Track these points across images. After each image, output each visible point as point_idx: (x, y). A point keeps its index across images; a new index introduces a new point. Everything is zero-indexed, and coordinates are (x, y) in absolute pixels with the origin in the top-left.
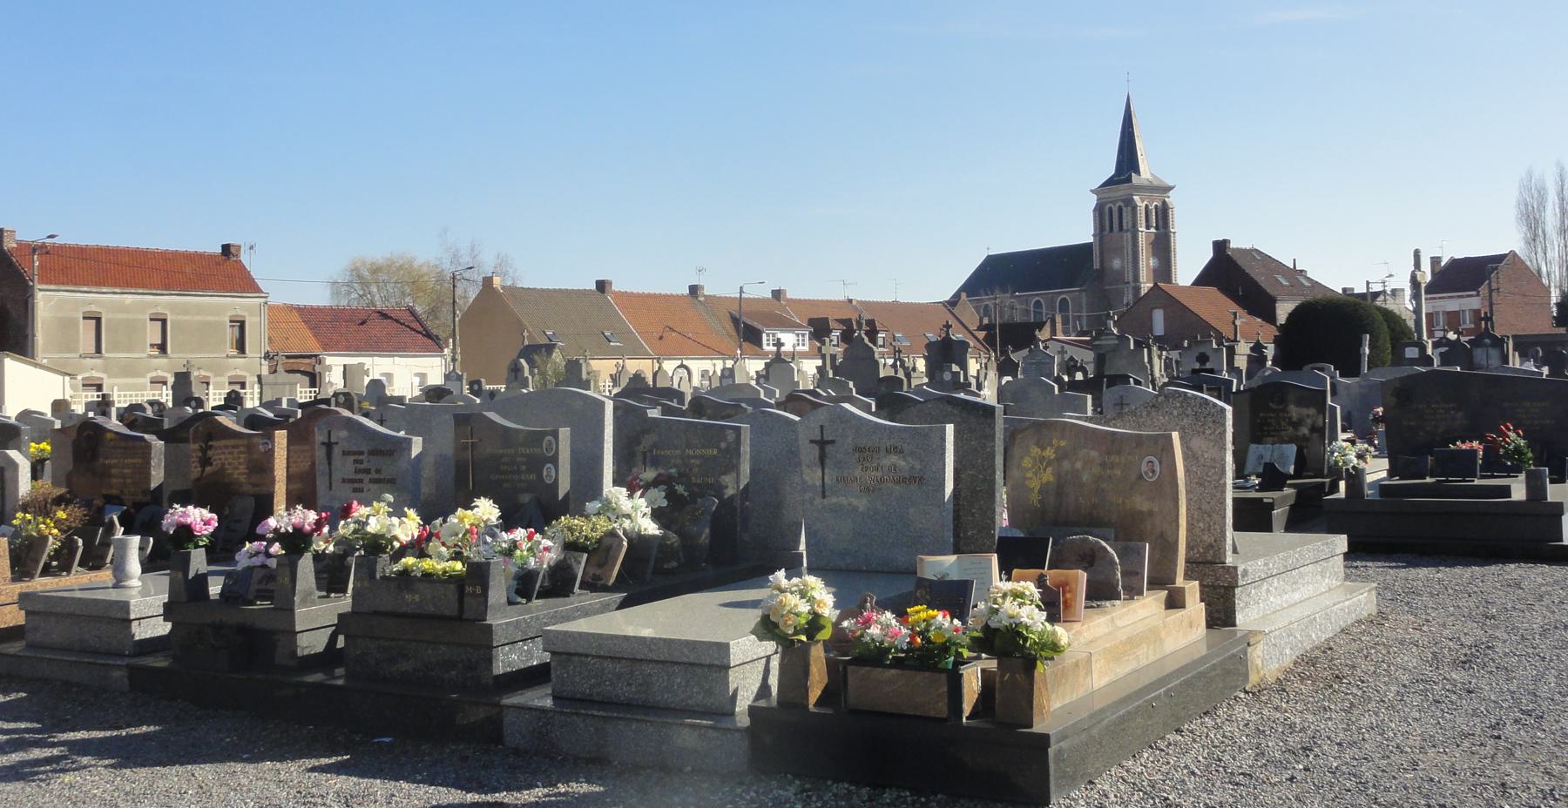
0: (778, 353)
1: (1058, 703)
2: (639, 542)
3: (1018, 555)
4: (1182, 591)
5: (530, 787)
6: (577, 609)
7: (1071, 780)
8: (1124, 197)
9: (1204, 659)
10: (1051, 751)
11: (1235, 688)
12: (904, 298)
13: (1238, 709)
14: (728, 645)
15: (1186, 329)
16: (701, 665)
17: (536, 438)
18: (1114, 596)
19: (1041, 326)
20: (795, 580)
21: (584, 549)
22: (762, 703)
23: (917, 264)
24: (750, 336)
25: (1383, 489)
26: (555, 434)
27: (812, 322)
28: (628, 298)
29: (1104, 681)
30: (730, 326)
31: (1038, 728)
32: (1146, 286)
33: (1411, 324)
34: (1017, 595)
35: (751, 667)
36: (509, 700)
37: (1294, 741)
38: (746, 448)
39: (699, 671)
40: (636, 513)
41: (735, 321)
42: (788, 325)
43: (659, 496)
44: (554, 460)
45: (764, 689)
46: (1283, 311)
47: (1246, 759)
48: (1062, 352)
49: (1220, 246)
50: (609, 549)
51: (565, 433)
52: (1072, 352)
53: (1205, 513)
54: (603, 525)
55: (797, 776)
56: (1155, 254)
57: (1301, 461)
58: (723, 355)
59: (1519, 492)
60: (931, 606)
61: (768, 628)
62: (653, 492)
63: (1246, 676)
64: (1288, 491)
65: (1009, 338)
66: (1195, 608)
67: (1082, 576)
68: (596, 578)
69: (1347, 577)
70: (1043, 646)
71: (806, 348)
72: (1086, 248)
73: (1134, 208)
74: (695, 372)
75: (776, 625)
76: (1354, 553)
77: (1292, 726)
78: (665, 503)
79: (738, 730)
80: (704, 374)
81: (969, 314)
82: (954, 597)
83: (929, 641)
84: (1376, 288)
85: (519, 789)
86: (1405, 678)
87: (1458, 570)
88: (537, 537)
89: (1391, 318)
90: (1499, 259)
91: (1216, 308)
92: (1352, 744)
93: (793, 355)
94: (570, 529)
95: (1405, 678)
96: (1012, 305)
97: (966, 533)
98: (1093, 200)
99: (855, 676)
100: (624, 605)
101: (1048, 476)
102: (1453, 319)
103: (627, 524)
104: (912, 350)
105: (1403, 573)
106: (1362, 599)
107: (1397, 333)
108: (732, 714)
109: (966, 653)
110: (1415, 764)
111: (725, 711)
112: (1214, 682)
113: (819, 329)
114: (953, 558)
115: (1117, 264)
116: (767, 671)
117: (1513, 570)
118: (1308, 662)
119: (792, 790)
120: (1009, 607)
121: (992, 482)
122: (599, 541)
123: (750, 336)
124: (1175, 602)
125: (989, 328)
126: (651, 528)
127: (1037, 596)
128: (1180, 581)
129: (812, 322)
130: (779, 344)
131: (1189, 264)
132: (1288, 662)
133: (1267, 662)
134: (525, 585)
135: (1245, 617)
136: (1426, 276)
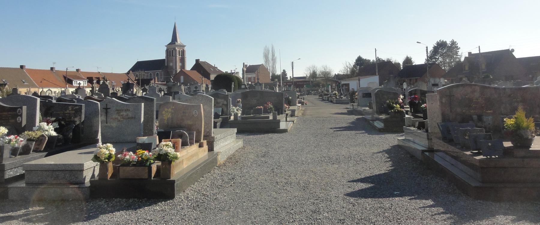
0: (79, 86)
1: (177, 172)
2: (51, 138)
3: (163, 135)
4: (203, 143)
5: (19, 210)
6: (32, 158)
7: (179, 191)
8: (173, 49)
9: (207, 160)
10: (175, 184)
11: (214, 166)
12: (114, 72)
13: (216, 171)
14: (83, 164)
15: (188, 80)
16: (74, 170)
17: (15, 109)
18: (187, 145)
19: (152, 80)
20: (104, 145)
21: (33, 140)
22: (93, 179)
23: (118, 63)
24: (69, 82)
25: (242, 118)
26: (21, 108)
27: (88, 78)
28: (31, 71)
29: (186, 166)
30: (63, 79)
31: (172, 179)
32: (179, 70)
33: (242, 80)
34: (167, 145)
35: (90, 169)
36: (10, 186)
37: (230, 177)
38: (83, 111)
39: (74, 172)
40: (50, 130)
41: (65, 78)
42: (81, 79)
43: (56, 125)
44: (21, 116)
45: (93, 175)
46: (213, 77)
47: (220, 182)
48: (158, 86)
49: (197, 61)
50: (41, 140)
51: (24, 108)
52: (160, 86)
53: (207, 124)
54: (39, 133)
55: (104, 198)
56: (181, 62)
57: (222, 111)
58: (61, 87)
59: (271, 118)
60: (143, 150)
61: (96, 158)
62: (54, 124)
63: (217, 163)
64: (220, 119)
65: (143, 83)
66: (206, 147)
67: (180, 140)
68: (38, 149)
69: (237, 138)
70: (173, 158)
71: (86, 85)
72: (163, 60)
73: (176, 50)
74: (55, 91)
75: (99, 158)
76: (239, 133)
77: (229, 173)
78: (58, 127)
79: (86, 187)
80: (55, 92)
81: (132, 77)
82: (147, 147)
83: (143, 158)
84: (233, 72)
85: (16, 211)
86: (252, 161)
87: (259, 136)
88: (18, 137)
89: (238, 78)
90: (260, 65)
91: (196, 76)
92: (243, 176)
93: (83, 87)
94: (29, 135)
95: (252, 161)
96: (144, 74)
97: (148, 132)
98: (165, 48)
99: (122, 169)
100: (46, 156)
101: (169, 116)
102: (249, 79)
103: (47, 133)
104: (117, 86)
105: (247, 137)
106: (240, 143)
107: (239, 83)
108: (84, 183)
109: (152, 161)
110: (257, 179)
111: (81, 183)
112: (211, 164)
113: (90, 80)
114: (146, 137)
115: (171, 64)
116: (94, 170)
117: (270, 135)
118: (230, 158)
119: (103, 202)
120: (165, 148)
121: (153, 118)
122: (38, 138)
123: (69, 82)
124: (201, 146)
125: (138, 80)
126: (54, 134)
127: (172, 145)
128: (202, 141)
129: (88, 78)
130: (80, 84)
131: (189, 65)
132: (225, 159)
133: (221, 159)
134: (14, 152)
135: (216, 149)
136: (245, 69)
